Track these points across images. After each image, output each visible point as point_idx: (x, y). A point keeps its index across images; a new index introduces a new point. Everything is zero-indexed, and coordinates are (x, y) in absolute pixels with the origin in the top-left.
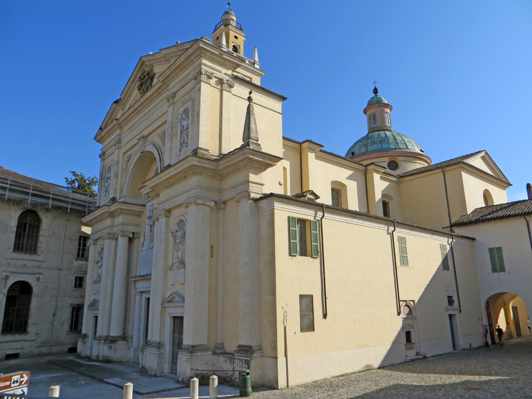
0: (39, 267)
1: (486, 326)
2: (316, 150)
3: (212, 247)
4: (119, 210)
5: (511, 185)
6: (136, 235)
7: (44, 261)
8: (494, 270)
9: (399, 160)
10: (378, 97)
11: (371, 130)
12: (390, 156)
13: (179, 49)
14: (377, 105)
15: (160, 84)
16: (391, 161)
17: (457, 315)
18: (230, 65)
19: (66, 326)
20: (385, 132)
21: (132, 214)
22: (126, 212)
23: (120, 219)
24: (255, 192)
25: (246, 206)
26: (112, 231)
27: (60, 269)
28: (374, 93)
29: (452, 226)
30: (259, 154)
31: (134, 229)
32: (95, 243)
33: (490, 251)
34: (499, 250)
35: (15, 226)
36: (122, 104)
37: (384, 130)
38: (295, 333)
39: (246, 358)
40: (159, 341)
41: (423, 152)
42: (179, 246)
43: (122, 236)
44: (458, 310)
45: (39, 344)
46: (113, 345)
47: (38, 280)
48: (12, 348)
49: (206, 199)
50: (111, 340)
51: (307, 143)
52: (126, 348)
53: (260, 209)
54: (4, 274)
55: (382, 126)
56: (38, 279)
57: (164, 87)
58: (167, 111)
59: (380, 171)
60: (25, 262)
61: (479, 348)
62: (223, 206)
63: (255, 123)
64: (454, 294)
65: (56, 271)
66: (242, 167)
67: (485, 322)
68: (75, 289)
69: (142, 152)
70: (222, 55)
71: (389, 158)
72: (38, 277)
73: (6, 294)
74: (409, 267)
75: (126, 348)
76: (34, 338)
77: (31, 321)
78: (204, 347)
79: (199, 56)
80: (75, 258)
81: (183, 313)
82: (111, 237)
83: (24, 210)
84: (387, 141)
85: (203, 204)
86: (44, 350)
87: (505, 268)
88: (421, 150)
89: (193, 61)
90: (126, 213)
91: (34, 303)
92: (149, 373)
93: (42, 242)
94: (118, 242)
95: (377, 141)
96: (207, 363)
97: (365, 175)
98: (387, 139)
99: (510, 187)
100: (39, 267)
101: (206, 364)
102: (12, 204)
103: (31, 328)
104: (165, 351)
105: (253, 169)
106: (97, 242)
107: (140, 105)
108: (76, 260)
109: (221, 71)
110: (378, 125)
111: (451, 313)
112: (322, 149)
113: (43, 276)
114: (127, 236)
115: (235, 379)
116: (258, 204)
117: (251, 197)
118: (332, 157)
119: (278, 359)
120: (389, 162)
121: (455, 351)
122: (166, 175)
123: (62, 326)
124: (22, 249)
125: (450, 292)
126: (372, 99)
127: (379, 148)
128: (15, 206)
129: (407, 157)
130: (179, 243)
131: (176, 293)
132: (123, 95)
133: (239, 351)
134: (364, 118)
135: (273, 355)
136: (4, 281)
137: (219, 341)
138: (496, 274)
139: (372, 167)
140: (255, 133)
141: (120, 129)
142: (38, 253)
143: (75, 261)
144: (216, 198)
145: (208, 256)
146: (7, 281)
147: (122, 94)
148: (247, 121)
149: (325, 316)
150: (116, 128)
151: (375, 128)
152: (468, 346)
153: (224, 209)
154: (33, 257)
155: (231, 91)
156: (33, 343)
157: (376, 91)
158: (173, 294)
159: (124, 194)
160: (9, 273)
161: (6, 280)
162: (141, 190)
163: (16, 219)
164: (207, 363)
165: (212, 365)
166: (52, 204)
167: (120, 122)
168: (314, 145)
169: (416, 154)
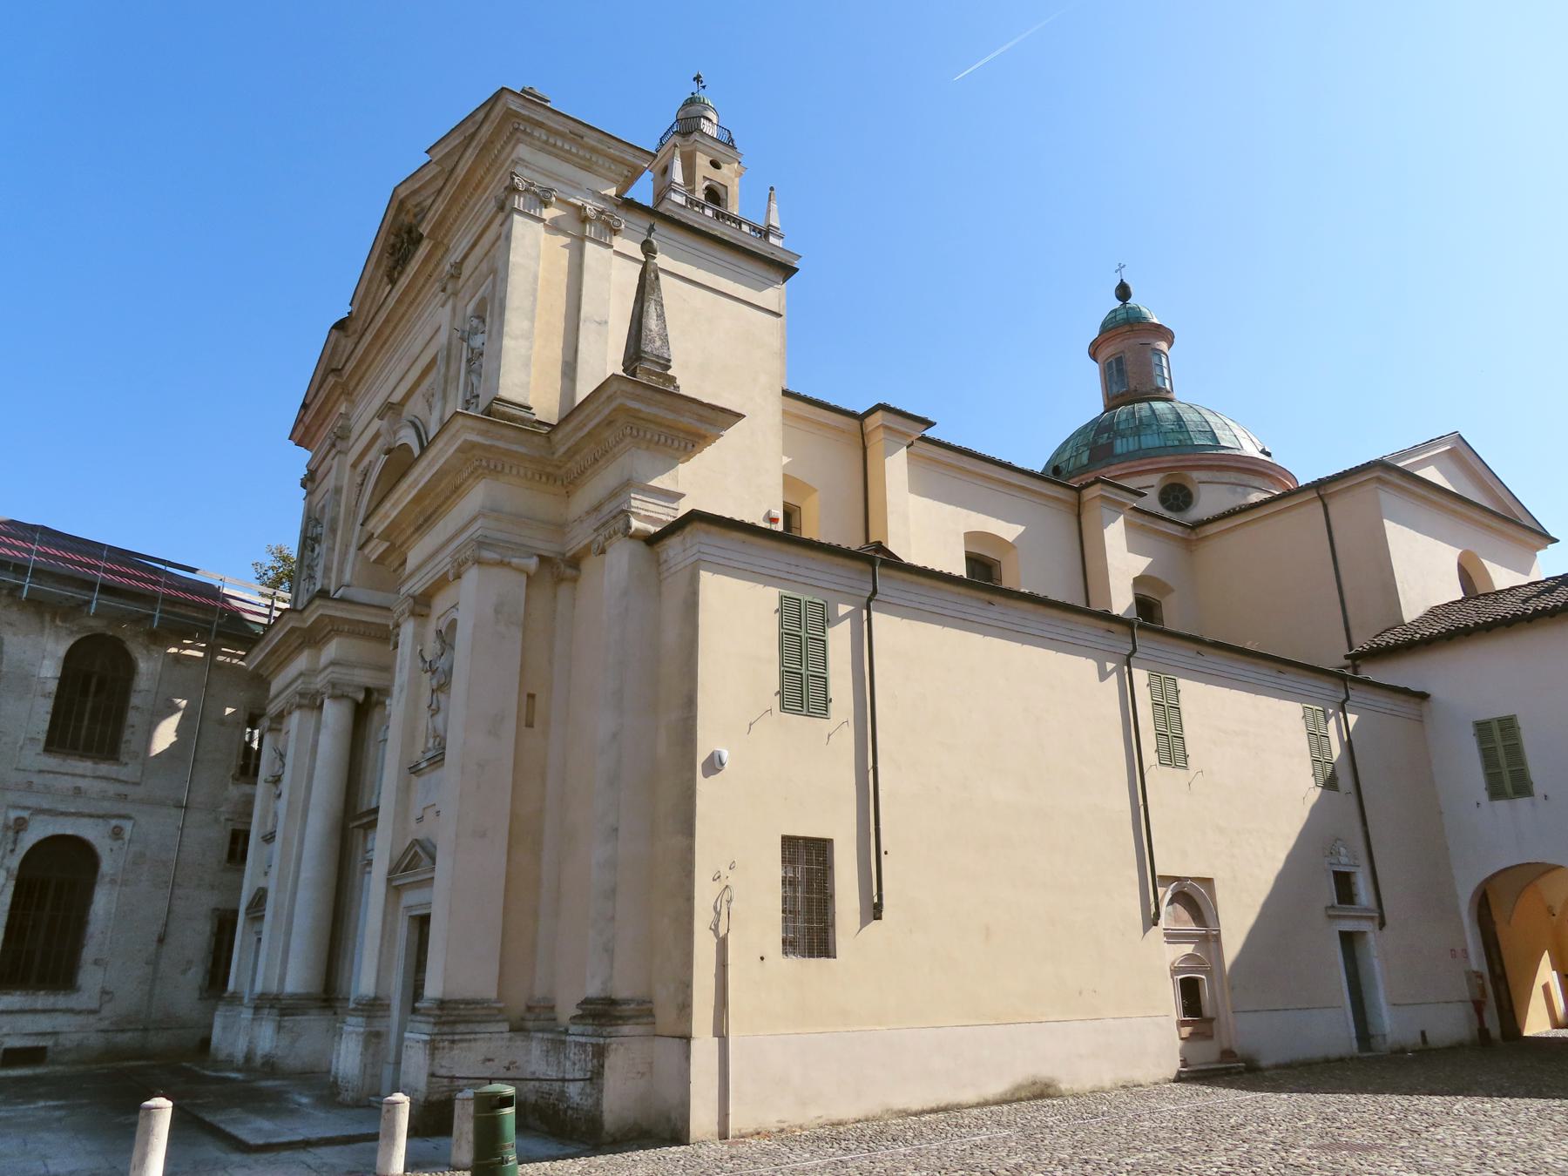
0: (123, 797)
1: (1480, 976)
2: (910, 436)
3: (531, 696)
4: (327, 620)
5: (1556, 541)
6: (375, 696)
7: (138, 780)
8: (1496, 792)
9: (1192, 478)
10: (1130, 308)
11: (1112, 402)
12: (1165, 468)
13: (467, 135)
14: (1127, 328)
15: (428, 245)
16: (1167, 486)
17: (1371, 936)
18: (604, 164)
19: (195, 976)
20: (1152, 403)
21: (358, 634)
22: (346, 627)
23: (332, 650)
24: (648, 514)
25: (619, 560)
26: (312, 686)
27: (186, 807)
28: (1119, 298)
29: (1357, 658)
30: (658, 397)
31: (365, 677)
32: (274, 726)
33: (1479, 730)
34: (1508, 725)
35: (56, 678)
36: (355, 332)
37: (1148, 400)
38: (762, 958)
39: (594, 1040)
40: (372, 994)
41: (1269, 454)
42: (438, 701)
43: (334, 697)
44: (1372, 918)
45: (112, 1023)
46: (288, 1021)
47: (116, 834)
48: (24, 1032)
49: (513, 549)
50: (281, 1007)
51: (879, 415)
52: (328, 1031)
53: (664, 567)
54: (13, 815)
55: (1144, 390)
56: (117, 833)
57: (439, 253)
58: (440, 327)
59: (1124, 505)
60: (81, 783)
61: (1455, 1049)
62: (569, 572)
63: (661, 316)
64: (1358, 866)
65: (174, 811)
66: (612, 442)
67: (1477, 962)
68: (228, 865)
69: (389, 452)
70: (582, 137)
71: (1162, 475)
72: (115, 827)
73: (16, 873)
74: (1192, 772)
75: (328, 1031)
76: (94, 1005)
77: (89, 953)
78: (483, 1008)
79: (513, 142)
80: (233, 776)
81: (429, 904)
82: (305, 702)
83: (78, 637)
84: (1155, 427)
85: (501, 564)
86: (124, 1039)
87: (1532, 783)
88: (1263, 452)
89: (499, 161)
90: (346, 630)
91: (102, 902)
92: (340, 1099)
93: (133, 726)
94: (323, 719)
95: (1126, 429)
96: (489, 1060)
97: (1079, 516)
98: (1155, 422)
99: (1550, 546)
100: (123, 797)
101: (487, 1063)
102: (47, 618)
103: (90, 978)
104: (388, 1026)
105: (648, 448)
106: (281, 723)
107: (387, 321)
108: (236, 779)
109: (579, 184)
110: (1132, 387)
111: (1348, 926)
112: (930, 433)
113: (134, 825)
114: (347, 697)
115: (565, 1111)
116: (658, 553)
117: (633, 529)
118: (965, 458)
119: (694, 1044)
120: (1162, 486)
121: (1365, 1055)
122: (407, 491)
123: (184, 972)
124: (76, 749)
125: (1341, 858)
126: (1114, 314)
127: (1131, 448)
128: (58, 622)
129: (1217, 471)
130: (437, 689)
131: (416, 842)
132: (356, 302)
133: (581, 1017)
134: (1093, 371)
135: (679, 1031)
136: (10, 834)
137: (539, 992)
138: (1502, 804)
139: (1096, 491)
140: (658, 343)
141: (346, 400)
142: (122, 758)
143: (233, 784)
144: (548, 548)
145: (511, 724)
146: (21, 834)
147: (355, 302)
148: (638, 309)
149: (874, 910)
150: (338, 399)
151: (1122, 395)
152: (1412, 1038)
153: (575, 580)
154: (105, 768)
155: (611, 241)
156: (92, 1019)
157: (1123, 292)
158: (414, 846)
159: (347, 577)
160: (30, 812)
161: (17, 832)
162: (367, 551)
163: (59, 658)
164: (489, 1060)
165: (507, 1065)
166: (160, 618)
167: (345, 378)
168: (900, 419)
169: (1246, 459)
